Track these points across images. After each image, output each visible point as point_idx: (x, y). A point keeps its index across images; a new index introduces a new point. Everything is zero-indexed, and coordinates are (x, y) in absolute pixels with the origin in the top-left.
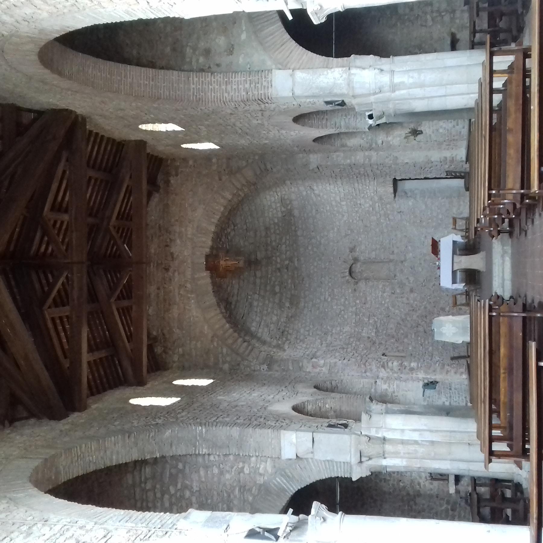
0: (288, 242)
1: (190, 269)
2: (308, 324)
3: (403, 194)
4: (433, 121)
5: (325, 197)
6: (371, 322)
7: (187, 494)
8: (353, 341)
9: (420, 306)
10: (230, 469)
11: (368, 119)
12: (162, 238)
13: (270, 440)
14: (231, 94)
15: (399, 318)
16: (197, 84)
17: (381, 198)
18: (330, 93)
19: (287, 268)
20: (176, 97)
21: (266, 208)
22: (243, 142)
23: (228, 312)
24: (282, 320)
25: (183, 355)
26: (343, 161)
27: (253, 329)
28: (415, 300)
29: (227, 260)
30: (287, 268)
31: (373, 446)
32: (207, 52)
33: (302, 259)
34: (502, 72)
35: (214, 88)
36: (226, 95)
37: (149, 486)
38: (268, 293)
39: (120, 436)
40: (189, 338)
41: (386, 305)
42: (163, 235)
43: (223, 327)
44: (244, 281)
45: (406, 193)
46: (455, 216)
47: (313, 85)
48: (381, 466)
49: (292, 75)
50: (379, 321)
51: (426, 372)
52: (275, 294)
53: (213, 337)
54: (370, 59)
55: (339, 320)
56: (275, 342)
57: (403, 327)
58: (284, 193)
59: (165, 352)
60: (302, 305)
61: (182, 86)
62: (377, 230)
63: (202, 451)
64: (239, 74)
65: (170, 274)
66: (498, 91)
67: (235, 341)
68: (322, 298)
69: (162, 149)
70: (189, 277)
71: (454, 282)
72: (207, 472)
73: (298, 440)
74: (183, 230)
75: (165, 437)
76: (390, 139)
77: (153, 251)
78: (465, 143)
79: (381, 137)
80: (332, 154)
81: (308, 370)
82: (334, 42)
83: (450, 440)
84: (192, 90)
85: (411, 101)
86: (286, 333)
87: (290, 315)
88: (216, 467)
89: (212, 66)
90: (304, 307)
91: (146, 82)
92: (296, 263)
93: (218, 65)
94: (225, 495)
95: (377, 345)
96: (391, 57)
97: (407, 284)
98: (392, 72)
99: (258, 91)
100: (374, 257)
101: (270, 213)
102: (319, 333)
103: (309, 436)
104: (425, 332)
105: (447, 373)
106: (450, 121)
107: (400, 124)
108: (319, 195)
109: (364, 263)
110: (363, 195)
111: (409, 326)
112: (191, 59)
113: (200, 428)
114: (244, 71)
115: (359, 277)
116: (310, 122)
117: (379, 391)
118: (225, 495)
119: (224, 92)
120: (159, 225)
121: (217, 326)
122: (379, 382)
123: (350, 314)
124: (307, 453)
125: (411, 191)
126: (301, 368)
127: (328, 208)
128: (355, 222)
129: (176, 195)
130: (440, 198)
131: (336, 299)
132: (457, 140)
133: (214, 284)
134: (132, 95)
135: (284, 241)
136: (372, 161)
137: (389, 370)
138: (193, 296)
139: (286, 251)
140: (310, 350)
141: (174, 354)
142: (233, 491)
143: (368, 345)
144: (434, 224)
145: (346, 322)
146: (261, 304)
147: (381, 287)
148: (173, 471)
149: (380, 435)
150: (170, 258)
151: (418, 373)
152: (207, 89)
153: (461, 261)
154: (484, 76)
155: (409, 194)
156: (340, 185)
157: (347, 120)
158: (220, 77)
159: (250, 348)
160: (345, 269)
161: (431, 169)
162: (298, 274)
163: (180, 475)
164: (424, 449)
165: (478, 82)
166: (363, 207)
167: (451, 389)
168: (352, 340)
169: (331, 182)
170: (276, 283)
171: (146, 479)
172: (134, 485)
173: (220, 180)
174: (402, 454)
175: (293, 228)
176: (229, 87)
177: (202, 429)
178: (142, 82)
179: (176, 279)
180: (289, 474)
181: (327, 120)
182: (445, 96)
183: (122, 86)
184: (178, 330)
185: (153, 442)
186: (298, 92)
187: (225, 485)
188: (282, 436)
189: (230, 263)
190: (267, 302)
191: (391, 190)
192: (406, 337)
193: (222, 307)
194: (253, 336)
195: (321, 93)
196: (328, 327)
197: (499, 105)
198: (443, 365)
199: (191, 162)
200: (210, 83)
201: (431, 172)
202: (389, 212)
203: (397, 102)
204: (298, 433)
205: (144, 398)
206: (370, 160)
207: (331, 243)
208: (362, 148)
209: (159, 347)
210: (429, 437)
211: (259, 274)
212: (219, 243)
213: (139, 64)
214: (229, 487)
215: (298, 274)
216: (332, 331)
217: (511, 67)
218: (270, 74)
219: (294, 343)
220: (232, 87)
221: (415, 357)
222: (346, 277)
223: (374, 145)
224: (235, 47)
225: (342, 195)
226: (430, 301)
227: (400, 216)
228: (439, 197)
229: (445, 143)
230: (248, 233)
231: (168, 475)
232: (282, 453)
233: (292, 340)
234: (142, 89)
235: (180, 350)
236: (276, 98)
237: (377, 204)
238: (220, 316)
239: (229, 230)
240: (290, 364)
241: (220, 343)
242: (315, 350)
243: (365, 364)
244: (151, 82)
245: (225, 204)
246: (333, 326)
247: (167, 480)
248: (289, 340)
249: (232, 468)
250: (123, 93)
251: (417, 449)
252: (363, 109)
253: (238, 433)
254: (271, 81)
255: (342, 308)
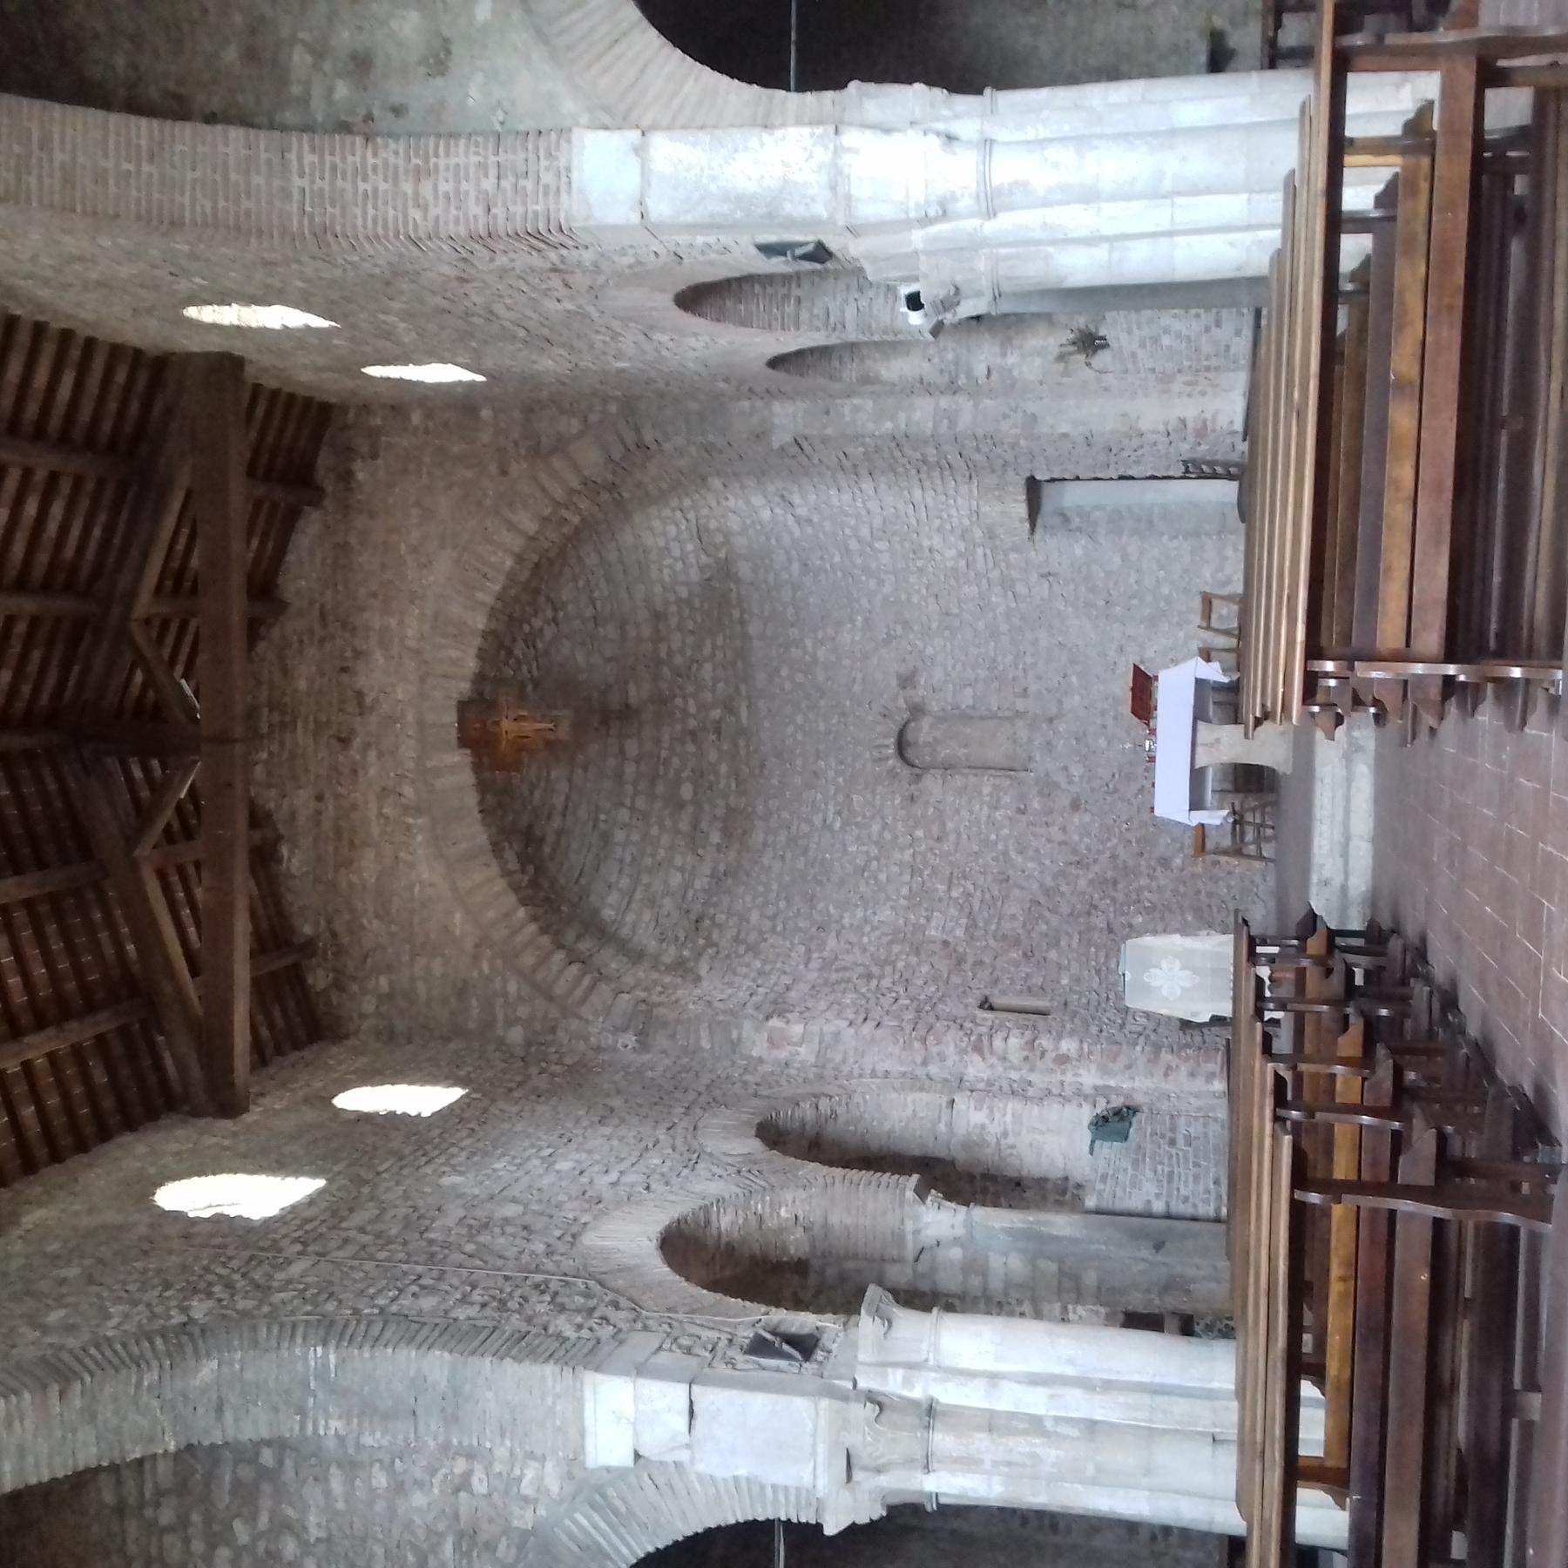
0: (720, 655)
1: (412, 742)
2: (773, 896)
3: (1057, 521)
4: (1137, 310)
5: (828, 526)
6: (954, 894)
7: (290, 1547)
8: (901, 952)
9: (1098, 852)
10: (427, 1478)
11: (905, 309)
12: (328, 646)
13: (549, 1401)
14: (433, 212)
15: (1035, 886)
16: (312, 174)
17: (991, 535)
18: (770, 216)
19: (718, 731)
20: (237, 218)
21: (653, 556)
22: (549, 364)
23: (531, 868)
24: (698, 884)
25: (390, 997)
26: (870, 426)
27: (608, 913)
28: (1085, 832)
29: (522, 718)
30: (718, 731)
31: (890, 1436)
32: (361, 64)
33: (761, 704)
34: (1380, 147)
35: (375, 190)
36: (415, 214)
37: (166, 1516)
38: (659, 804)
39: (27, 1395)
40: (407, 947)
41: (1000, 847)
42: (333, 637)
43: (508, 915)
44: (585, 769)
45: (1065, 519)
46: (1207, 589)
47: (713, 188)
48: (921, 1493)
49: (639, 151)
50: (978, 893)
51: (1104, 1071)
52: (681, 805)
53: (477, 946)
54: (915, 98)
55: (862, 889)
56: (670, 954)
57: (1047, 914)
58: (705, 512)
59: (338, 985)
60: (758, 837)
61: (258, 180)
62: (981, 625)
63: (327, 1427)
64: (462, 142)
65: (355, 753)
66: (1360, 223)
67: (543, 960)
68: (817, 820)
69: (305, 376)
70: (411, 765)
71: (1196, 804)
72: (352, 1483)
73: (641, 1407)
74: (393, 622)
75: (196, 1382)
76: (1011, 360)
77: (302, 685)
78: (1241, 379)
79: (984, 355)
80: (839, 401)
81: (755, 1053)
82: (793, 37)
83: (1151, 1421)
84: (296, 196)
85: (1051, 249)
86: (707, 922)
87: (722, 867)
88: (382, 1467)
89: (376, 113)
90: (765, 844)
91: (125, 166)
92: (744, 713)
93: (398, 111)
94: (411, 1558)
95: (967, 966)
96: (988, 91)
97: (1064, 785)
98: (988, 144)
99: (525, 204)
100: (970, 702)
101: (666, 571)
102: (802, 924)
103: (676, 1394)
104: (1110, 930)
105: (1166, 1075)
106: (1193, 311)
107: (1047, 318)
108: (809, 521)
109: (943, 719)
110: (938, 522)
111: (1065, 910)
112: (307, 85)
113: (319, 1349)
114: (477, 134)
115: (928, 758)
116: (742, 307)
117: (961, 1129)
118: (411, 1558)
119: (410, 203)
120: (322, 607)
121: (491, 914)
122: (961, 1104)
123: (896, 869)
124: (673, 1449)
125: (1081, 512)
126: (735, 1045)
127: (837, 559)
128: (915, 599)
129: (372, 515)
130: (1165, 538)
131: (857, 824)
132: (1217, 369)
133: (483, 787)
134: (73, 211)
135: (707, 650)
136: (960, 428)
137: (994, 1060)
138: (420, 821)
139: (716, 680)
140: (773, 979)
141: (364, 991)
142: (435, 1548)
143: (943, 966)
144: (1147, 612)
145: (882, 896)
146: (635, 837)
147: (986, 790)
148: (246, 1472)
149: (916, 1393)
150: (351, 707)
151: (1081, 1071)
152: (349, 195)
153: (1218, 740)
154: (1306, 163)
155: (1076, 522)
156: (871, 492)
157: (864, 303)
158: (396, 153)
159: (587, 980)
160: (885, 737)
161: (1140, 452)
162: (747, 746)
163: (267, 1488)
164: (1061, 1453)
165: (1281, 186)
166: (938, 557)
167: (1173, 1142)
168: (896, 948)
169: (844, 484)
170: (684, 775)
171: (160, 1494)
172: (120, 1510)
173: (504, 472)
174: (988, 1465)
175: (736, 614)
176: (426, 188)
177: (326, 1355)
178: (110, 164)
179: (372, 772)
180: (618, 1503)
181: (799, 300)
182: (1170, 234)
183: (33, 180)
184: (376, 923)
185: (155, 1403)
186: (660, 209)
187: (408, 1526)
188: (588, 1394)
189: (528, 727)
190: (655, 830)
191: (1021, 509)
192: (1056, 944)
193: (510, 855)
194: (604, 934)
195: (739, 214)
196: (831, 908)
197: (1362, 273)
198: (1157, 1048)
199: (416, 418)
200: (361, 173)
201: (1137, 462)
202: (1015, 574)
203: (1003, 251)
204: (641, 1381)
205: (211, 1177)
206: (952, 424)
207: (846, 662)
208: (925, 387)
209: (320, 973)
210: (1080, 1405)
211: (632, 747)
212: (506, 664)
213: (136, 106)
214: (421, 1533)
215: (747, 746)
216: (842, 917)
217: (1417, 126)
218: (564, 144)
219: (728, 957)
220: (435, 188)
221: (1074, 1014)
222: (887, 759)
223: (962, 381)
224: (454, 49)
225: (877, 522)
226: (1128, 835)
227: (1046, 585)
228: (1163, 534)
229: (1181, 378)
230: (600, 630)
231: (227, 1487)
232: (589, 1446)
233: (723, 943)
234: (112, 188)
235: (383, 981)
236: (585, 229)
237: (980, 551)
238: (500, 884)
239: (537, 623)
240: (704, 1034)
241: (499, 962)
242: (786, 980)
243: (924, 1040)
244: (146, 168)
245: (517, 549)
246: (844, 905)
247: (223, 1499)
248: (715, 945)
249: (433, 1472)
250: (35, 204)
251: (1039, 1450)
252: (893, 274)
253: (446, 1372)
254: (568, 169)
255: (874, 851)
